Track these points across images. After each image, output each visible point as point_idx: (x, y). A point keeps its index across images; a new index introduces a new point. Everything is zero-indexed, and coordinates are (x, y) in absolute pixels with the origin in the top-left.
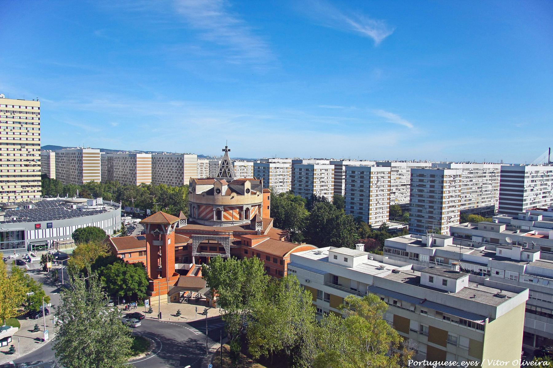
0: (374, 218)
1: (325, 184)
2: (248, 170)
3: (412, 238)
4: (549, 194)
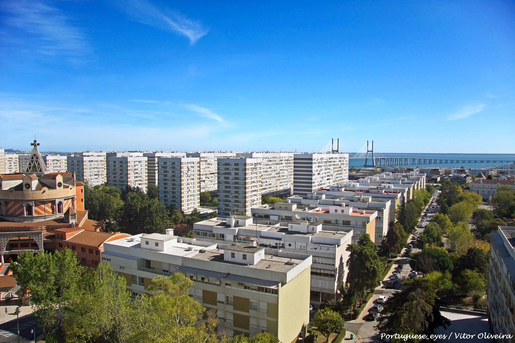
0: (187, 205)
1: (139, 175)
2: (61, 164)
3: (218, 221)
4: (332, 177)
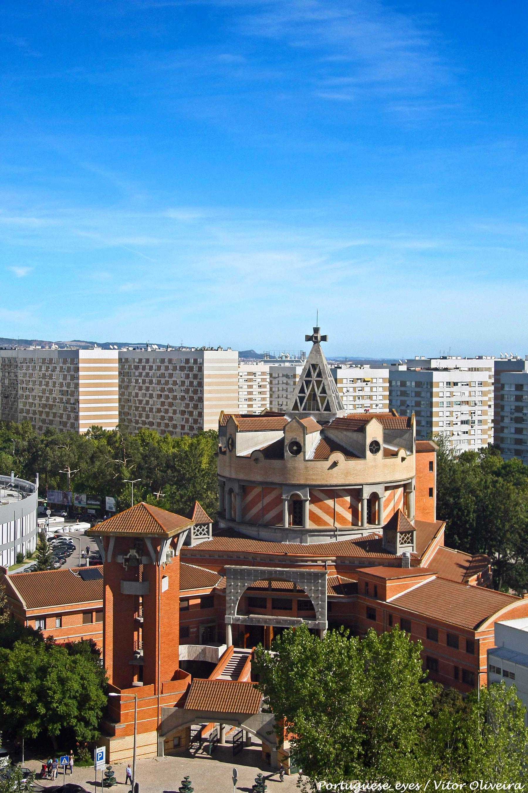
2: (374, 389)
